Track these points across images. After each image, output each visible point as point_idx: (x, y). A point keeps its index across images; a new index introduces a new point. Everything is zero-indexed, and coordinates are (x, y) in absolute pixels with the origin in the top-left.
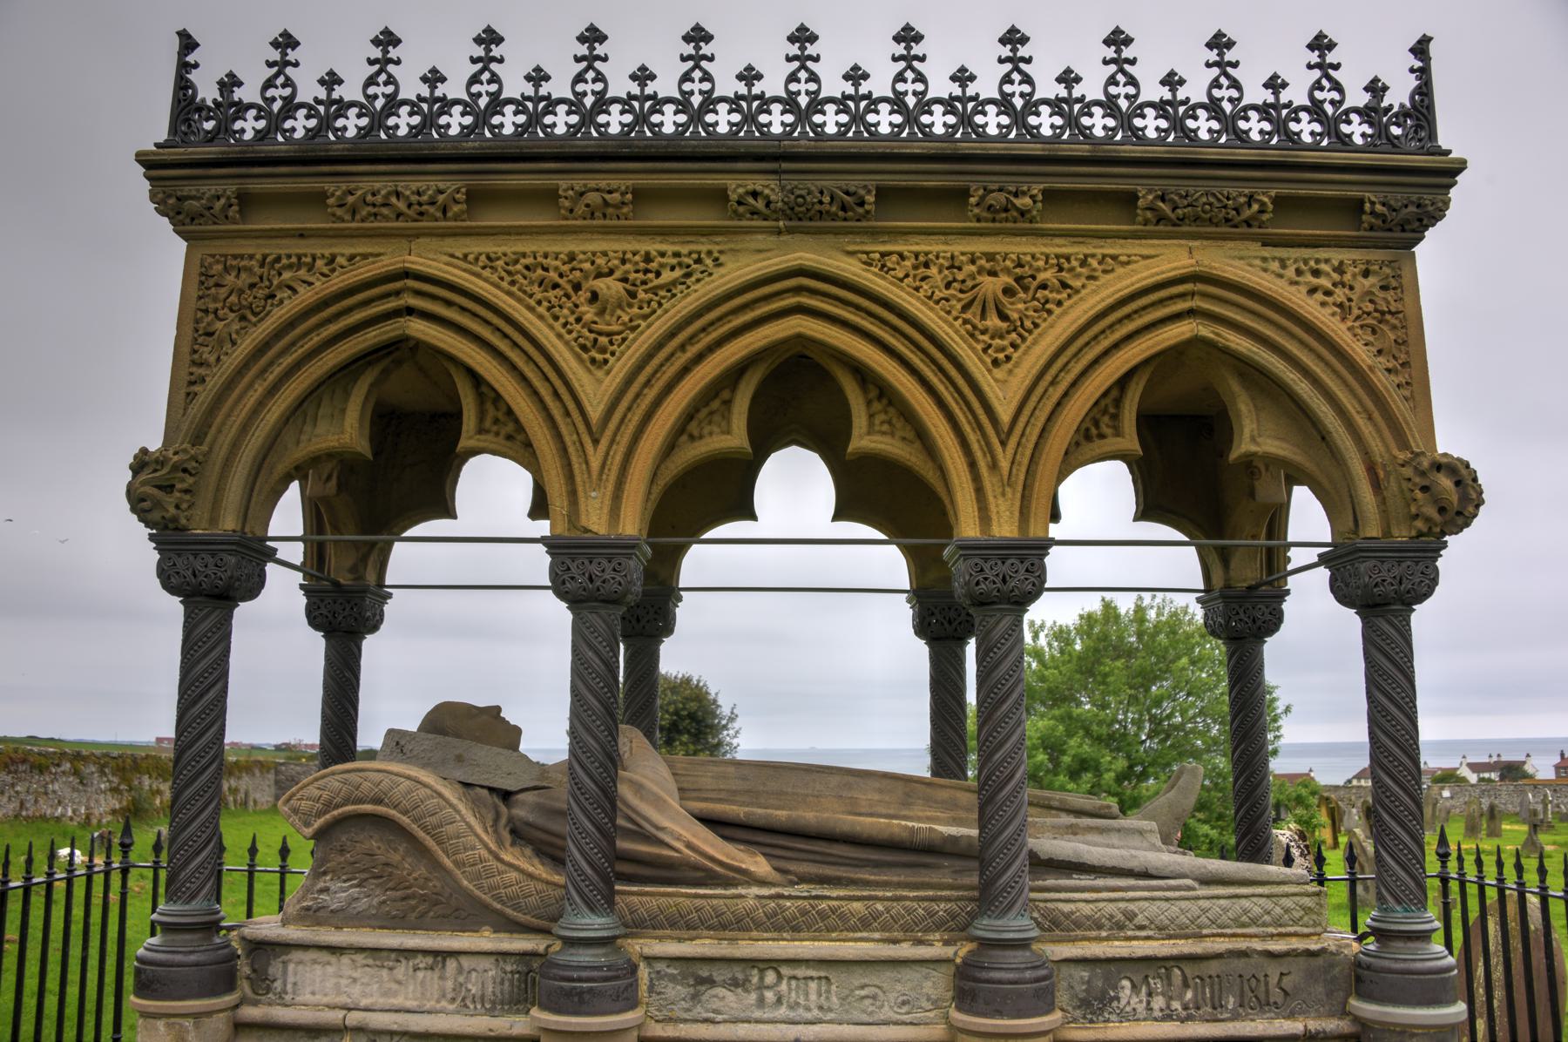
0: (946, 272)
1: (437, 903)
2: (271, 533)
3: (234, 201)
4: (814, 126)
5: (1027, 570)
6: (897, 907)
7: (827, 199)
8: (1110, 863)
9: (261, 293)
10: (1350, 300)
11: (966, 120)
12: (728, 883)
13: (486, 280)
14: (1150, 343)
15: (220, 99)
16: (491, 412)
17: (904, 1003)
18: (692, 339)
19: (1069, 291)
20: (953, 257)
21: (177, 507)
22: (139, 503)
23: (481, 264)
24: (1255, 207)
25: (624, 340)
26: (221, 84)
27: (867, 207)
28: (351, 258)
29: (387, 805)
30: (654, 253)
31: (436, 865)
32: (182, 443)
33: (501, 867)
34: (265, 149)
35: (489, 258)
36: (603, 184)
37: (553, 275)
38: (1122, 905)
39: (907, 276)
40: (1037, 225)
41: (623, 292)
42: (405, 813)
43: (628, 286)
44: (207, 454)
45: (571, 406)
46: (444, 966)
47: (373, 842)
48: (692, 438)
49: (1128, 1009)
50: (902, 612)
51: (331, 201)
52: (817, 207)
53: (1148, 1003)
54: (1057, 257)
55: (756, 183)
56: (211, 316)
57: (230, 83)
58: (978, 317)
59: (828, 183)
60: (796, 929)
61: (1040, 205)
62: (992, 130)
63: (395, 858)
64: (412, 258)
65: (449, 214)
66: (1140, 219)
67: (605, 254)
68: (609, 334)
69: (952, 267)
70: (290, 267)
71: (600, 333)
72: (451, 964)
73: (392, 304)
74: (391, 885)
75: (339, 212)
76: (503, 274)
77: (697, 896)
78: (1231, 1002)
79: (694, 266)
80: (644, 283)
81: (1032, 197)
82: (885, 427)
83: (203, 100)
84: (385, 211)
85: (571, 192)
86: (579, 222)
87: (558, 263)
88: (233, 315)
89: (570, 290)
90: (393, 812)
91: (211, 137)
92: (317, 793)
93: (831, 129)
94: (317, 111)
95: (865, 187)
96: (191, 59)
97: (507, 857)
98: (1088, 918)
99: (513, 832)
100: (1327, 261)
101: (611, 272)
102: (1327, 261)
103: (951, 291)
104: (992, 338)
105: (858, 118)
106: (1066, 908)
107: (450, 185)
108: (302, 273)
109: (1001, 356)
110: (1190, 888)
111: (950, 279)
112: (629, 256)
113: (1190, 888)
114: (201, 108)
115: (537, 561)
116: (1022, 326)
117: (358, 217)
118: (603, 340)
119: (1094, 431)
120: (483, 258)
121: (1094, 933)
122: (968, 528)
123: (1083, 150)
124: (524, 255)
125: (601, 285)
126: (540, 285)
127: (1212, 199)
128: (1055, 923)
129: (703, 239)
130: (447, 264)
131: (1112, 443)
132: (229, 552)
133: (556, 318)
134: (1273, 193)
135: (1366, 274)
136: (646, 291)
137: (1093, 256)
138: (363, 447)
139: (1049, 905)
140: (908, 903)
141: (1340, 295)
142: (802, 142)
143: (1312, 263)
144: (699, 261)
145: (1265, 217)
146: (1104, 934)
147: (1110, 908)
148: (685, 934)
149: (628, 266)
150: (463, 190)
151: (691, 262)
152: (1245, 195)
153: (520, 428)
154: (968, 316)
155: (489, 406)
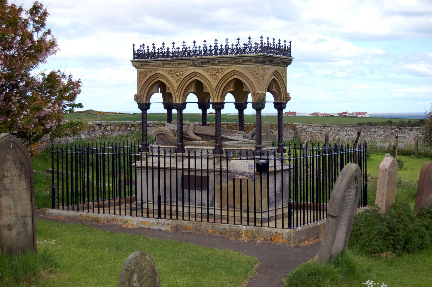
6: (211, 143)
8: (234, 139)
9: (145, 75)
12: (196, 140)
31: (168, 139)
44: (141, 94)
47: (162, 136)
90: (164, 133)
106: (227, 144)
107: (161, 63)
118: (178, 80)
147: (232, 144)
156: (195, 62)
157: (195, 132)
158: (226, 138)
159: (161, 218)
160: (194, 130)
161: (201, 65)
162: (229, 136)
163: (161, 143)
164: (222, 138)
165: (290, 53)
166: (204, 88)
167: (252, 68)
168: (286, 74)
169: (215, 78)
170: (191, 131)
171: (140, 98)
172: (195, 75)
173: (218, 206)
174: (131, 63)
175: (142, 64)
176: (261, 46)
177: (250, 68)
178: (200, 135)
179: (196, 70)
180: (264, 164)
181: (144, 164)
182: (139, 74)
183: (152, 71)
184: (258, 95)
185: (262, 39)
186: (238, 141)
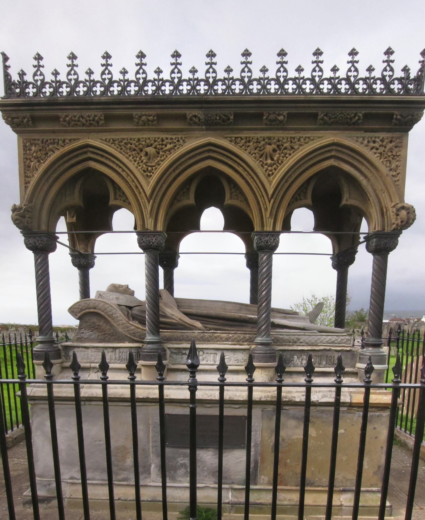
0: (255, 144)
1: (113, 335)
2: (57, 231)
3: (30, 119)
4: (215, 90)
5: (274, 239)
6: (236, 336)
7: (218, 118)
8: (294, 326)
9: (44, 152)
11: (264, 87)
12: (190, 329)
13: (113, 148)
14: (317, 168)
15: (20, 80)
16: (118, 193)
17: (236, 360)
18: (177, 168)
19: (293, 150)
20: (257, 139)
21: (27, 223)
23: (111, 142)
24: (357, 118)
25: (156, 168)
26: (19, 74)
27: (231, 121)
28: (70, 140)
29: (97, 309)
30: (164, 138)
31: (112, 326)
32: (26, 202)
33: (129, 325)
34: (37, 99)
35: (113, 140)
36: (147, 113)
37: (133, 146)
38: (296, 336)
39: (243, 145)
41: (155, 151)
42: (103, 311)
43: (157, 150)
45: (141, 191)
46: (115, 351)
47: (94, 320)
48: (178, 201)
49: (296, 363)
50: (243, 260)
51: (61, 119)
52: (215, 121)
53: (301, 362)
54: (291, 138)
56: (29, 161)
57: (22, 74)
58: (265, 160)
59: (218, 112)
61: (286, 119)
62: (273, 91)
63: (101, 324)
64: (89, 140)
65: (99, 125)
66: (318, 123)
67: (149, 139)
68: (152, 166)
70: (51, 143)
71: (149, 166)
72: (117, 351)
74: (100, 331)
75: (64, 123)
76: (118, 146)
77: (182, 332)
78: (324, 363)
79: (177, 143)
80: (162, 149)
81: (284, 116)
82: (236, 197)
83: (14, 81)
84: (79, 123)
85: (137, 116)
86: (140, 127)
87: (134, 142)
88: (36, 160)
89: (139, 152)
90: (100, 312)
91: (19, 95)
92: (78, 307)
93: (220, 92)
95: (230, 113)
96: (7, 64)
97: (130, 323)
98: (287, 339)
99: (133, 317)
100: (378, 137)
101: (151, 145)
102: (378, 137)
103: (257, 151)
104: (269, 167)
105: (229, 87)
106: (281, 337)
107: (99, 114)
108: (55, 145)
109: (270, 173)
110: (315, 333)
111: (256, 146)
112: (156, 139)
113: (315, 333)
114: (14, 84)
116: (278, 163)
117: (71, 125)
118: (149, 168)
119: (298, 198)
120: (111, 140)
121: (288, 344)
123: (302, 97)
124: (124, 139)
125: (148, 149)
126: (130, 150)
127: (342, 115)
128: (278, 340)
129: (180, 133)
130: (101, 142)
131: (304, 202)
132: (45, 236)
133: (135, 161)
134: (363, 112)
135: (391, 142)
136: (162, 152)
137: (302, 137)
138: (81, 204)
140: (238, 335)
141: (381, 150)
142: (210, 97)
143: (373, 139)
144: (178, 141)
145: (360, 121)
146: (291, 344)
148: (178, 342)
149: (156, 143)
150: (103, 115)
151: (176, 141)
152: (354, 114)
153: (127, 198)
154: (261, 159)
155: (117, 191)
169: (271, 165)
172: (207, 155)
179: (213, 140)
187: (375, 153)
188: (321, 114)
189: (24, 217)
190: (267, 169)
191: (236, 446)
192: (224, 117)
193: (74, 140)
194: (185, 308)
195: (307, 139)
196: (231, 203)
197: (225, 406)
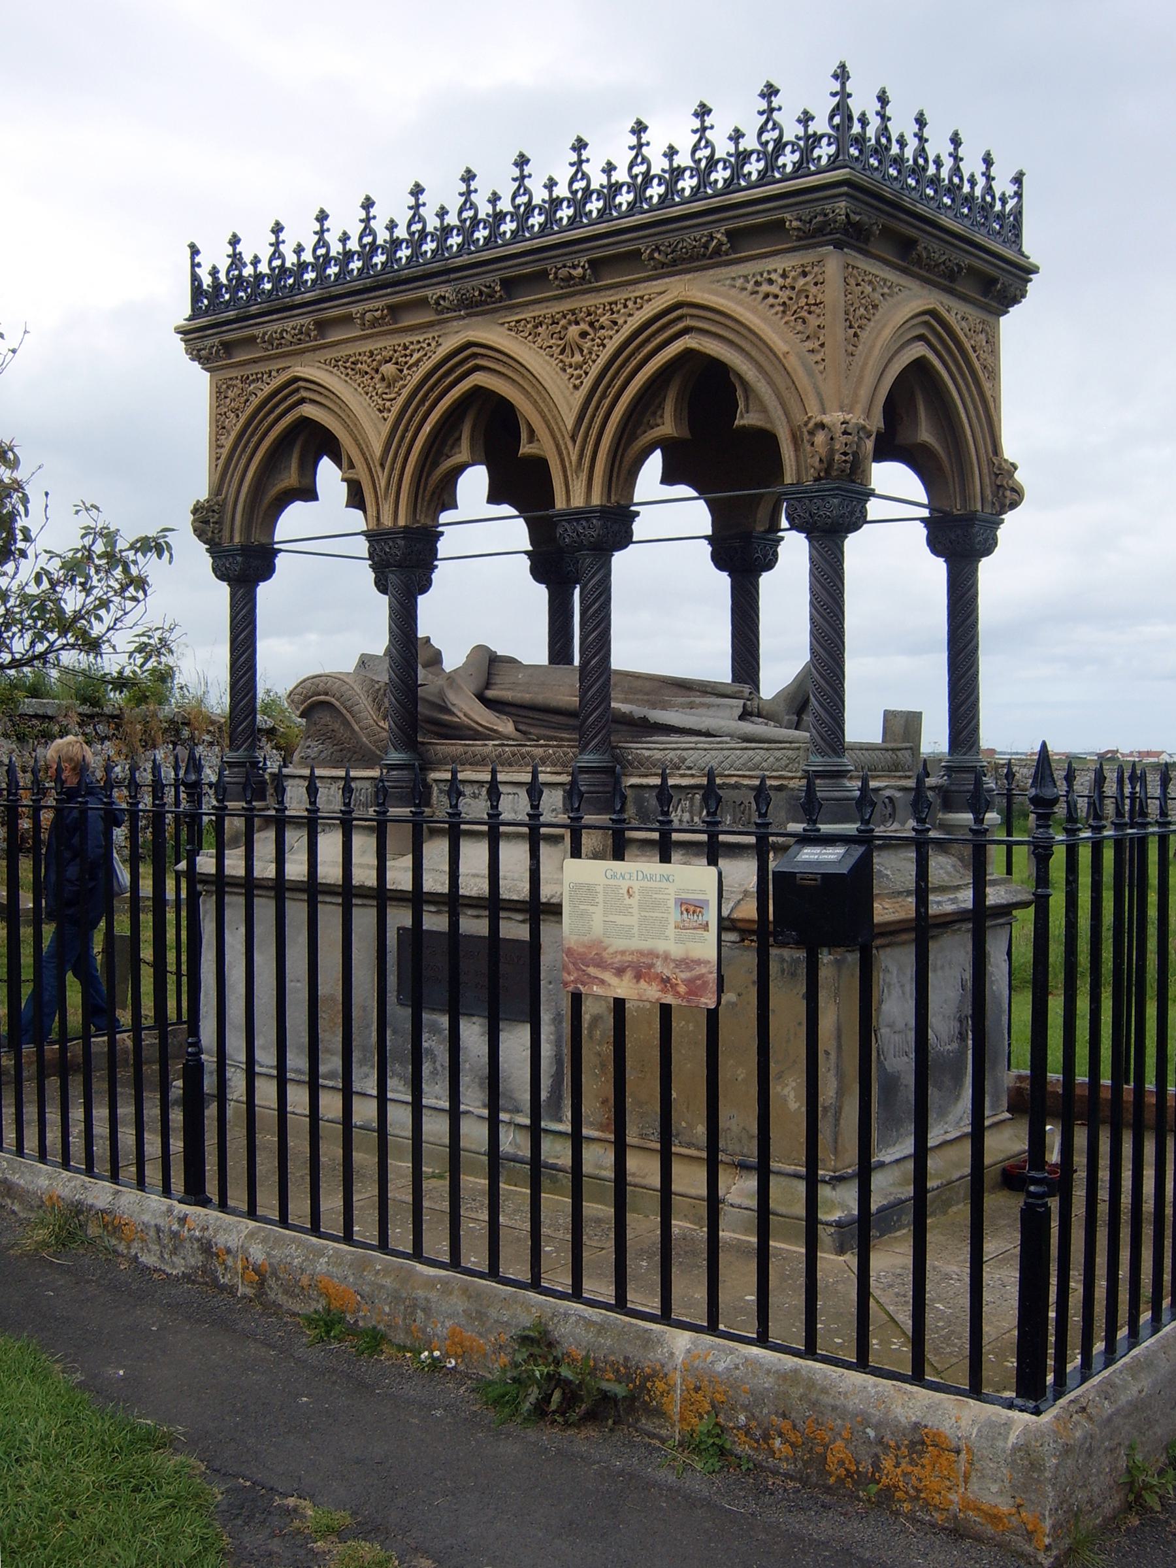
2: (276, 539)
6: (560, 751)
7: (476, 294)
10: (791, 299)
22: (200, 533)
28: (278, 371)
30: (407, 344)
31: (353, 730)
36: (371, 306)
38: (679, 752)
40: (593, 285)
51: (258, 341)
52: (474, 299)
54: (610, 304)
55: (441, 290)
60: (510, 765)
69: (553, 323)
73: (680, 326)
77: (466, 745)
80: (406, 363)
81: (583, 267)
84: (283, 341)
87: (365, 358)
90: (333, 700)
94: (799, 146)
96: (197, 259)
100: (775, 271)
102: (775, 271)
106: (647, 753)
107: (306, 321)
109: (578, 382)
115: (361, 546)
118: (388, 404)
122: (560, 504)
132: (834, 496)
134: (723, 230)
135: (805, 274)
137: (630, 299)
139: (638, 751)
144: (429, 345)
156: (469, 286)
157: (490, 694)
158: (645, 719)
159: (205, 1203)
160: (488, 685)
161: (501, 299)
162: (664, 709)
163: (323, 755)
164: (615, 721)
165: (1018, 236)
166: (524, 436)
167: (784, 275)
168: (995, 352)
170: (465, 688)
171: (217, 516)
173: (602, 1128)
174: (178, 345)
175: (228, 337)
176: (836, 128)
177: (771, 282)
178: (513, 710)
180: (829, 880)
181: (234, 867)
182: (219, 394)
183: (274, 373)
184: (820, 438)
185: (843, 85)
186: (708, 734)
187: (772, 306)
188: (646, 249)
189: (207, 522)
190: (572, 375)
191: (516, 1019)
192: (485, 290)
193: (284, 369)
194: (502, 689)
195: (639, 300)
196: (529, 451)
197: (502, 914)
